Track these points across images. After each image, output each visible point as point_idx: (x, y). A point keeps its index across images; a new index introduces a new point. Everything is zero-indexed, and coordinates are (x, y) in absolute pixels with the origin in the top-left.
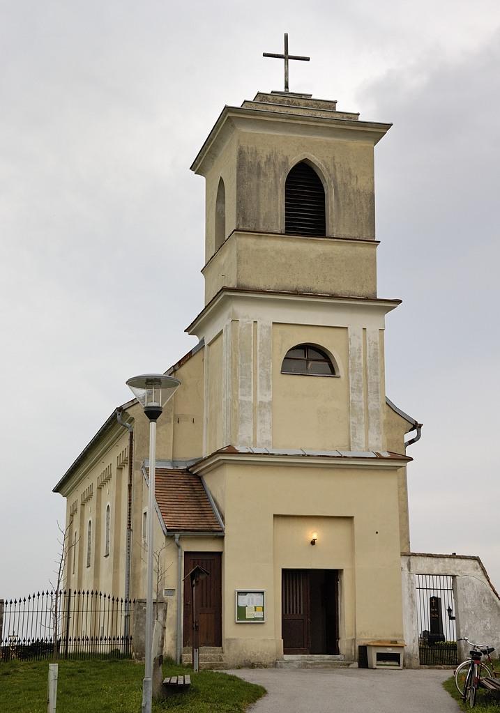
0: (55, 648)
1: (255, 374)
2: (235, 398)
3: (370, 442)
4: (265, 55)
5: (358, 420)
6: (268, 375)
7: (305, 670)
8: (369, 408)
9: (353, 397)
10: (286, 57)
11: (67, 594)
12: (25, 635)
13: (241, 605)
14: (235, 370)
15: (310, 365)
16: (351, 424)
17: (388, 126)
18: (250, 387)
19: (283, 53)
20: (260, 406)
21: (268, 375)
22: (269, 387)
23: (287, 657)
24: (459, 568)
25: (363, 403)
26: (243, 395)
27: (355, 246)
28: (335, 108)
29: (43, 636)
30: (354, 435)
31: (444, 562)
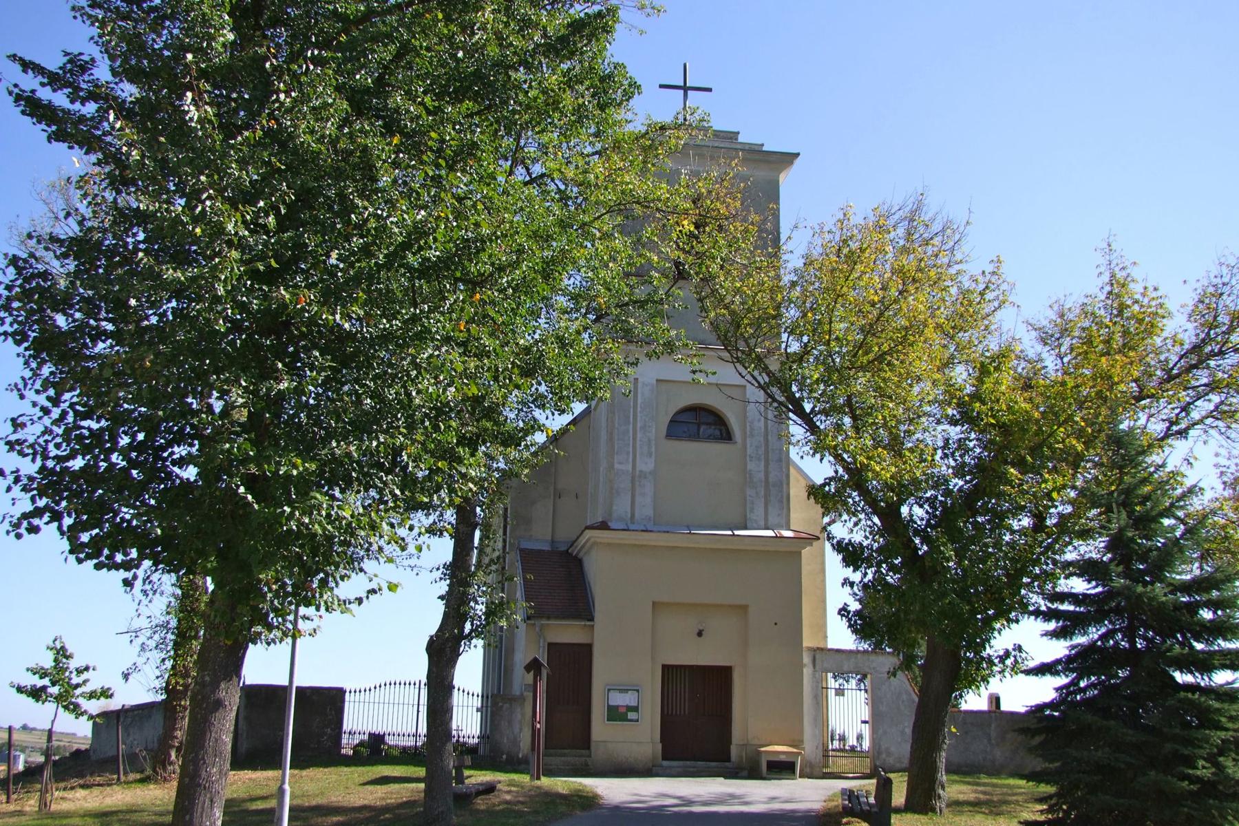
0: (573, 758)
1: (634, 439)
2: (611, 466)
3: (770, 518)
4: (661, 86)
5: (757, 493)
6: (649, 440)
7: (24, 744)
8: (770, 480)
9: (751, 466)
10: (685, 89)
11: (417, 686)
12: (404, 730)
13: (611, 703)
14: (611, 434)
15: (702, 430)
16: (748, 498)
17: (798, 154)
18: (628, 453)
19: (682, 84)
20: (640, 476)
21: (649, 440)
22: (650, 455)
23: (665, 763)
24: (874, 665)
25: (763, 473)
26: (620, 463)
27: (961, 813)
28: (737, 139)
29: (385, 729)
30: (752, 510)
31: (856, 658)
